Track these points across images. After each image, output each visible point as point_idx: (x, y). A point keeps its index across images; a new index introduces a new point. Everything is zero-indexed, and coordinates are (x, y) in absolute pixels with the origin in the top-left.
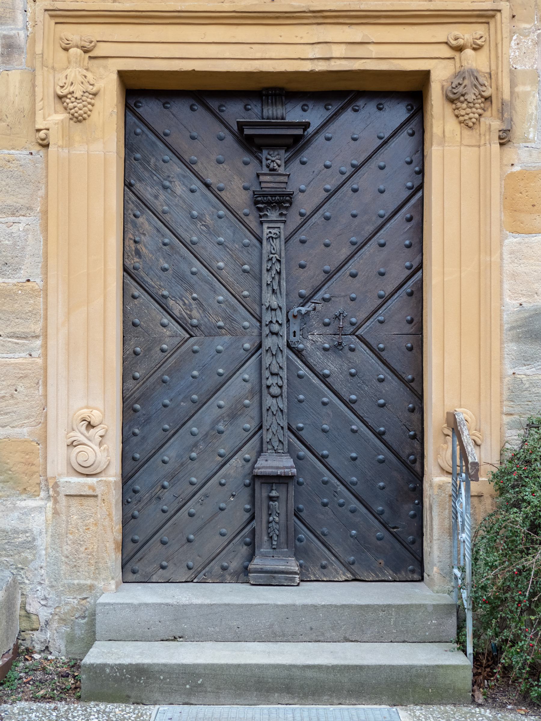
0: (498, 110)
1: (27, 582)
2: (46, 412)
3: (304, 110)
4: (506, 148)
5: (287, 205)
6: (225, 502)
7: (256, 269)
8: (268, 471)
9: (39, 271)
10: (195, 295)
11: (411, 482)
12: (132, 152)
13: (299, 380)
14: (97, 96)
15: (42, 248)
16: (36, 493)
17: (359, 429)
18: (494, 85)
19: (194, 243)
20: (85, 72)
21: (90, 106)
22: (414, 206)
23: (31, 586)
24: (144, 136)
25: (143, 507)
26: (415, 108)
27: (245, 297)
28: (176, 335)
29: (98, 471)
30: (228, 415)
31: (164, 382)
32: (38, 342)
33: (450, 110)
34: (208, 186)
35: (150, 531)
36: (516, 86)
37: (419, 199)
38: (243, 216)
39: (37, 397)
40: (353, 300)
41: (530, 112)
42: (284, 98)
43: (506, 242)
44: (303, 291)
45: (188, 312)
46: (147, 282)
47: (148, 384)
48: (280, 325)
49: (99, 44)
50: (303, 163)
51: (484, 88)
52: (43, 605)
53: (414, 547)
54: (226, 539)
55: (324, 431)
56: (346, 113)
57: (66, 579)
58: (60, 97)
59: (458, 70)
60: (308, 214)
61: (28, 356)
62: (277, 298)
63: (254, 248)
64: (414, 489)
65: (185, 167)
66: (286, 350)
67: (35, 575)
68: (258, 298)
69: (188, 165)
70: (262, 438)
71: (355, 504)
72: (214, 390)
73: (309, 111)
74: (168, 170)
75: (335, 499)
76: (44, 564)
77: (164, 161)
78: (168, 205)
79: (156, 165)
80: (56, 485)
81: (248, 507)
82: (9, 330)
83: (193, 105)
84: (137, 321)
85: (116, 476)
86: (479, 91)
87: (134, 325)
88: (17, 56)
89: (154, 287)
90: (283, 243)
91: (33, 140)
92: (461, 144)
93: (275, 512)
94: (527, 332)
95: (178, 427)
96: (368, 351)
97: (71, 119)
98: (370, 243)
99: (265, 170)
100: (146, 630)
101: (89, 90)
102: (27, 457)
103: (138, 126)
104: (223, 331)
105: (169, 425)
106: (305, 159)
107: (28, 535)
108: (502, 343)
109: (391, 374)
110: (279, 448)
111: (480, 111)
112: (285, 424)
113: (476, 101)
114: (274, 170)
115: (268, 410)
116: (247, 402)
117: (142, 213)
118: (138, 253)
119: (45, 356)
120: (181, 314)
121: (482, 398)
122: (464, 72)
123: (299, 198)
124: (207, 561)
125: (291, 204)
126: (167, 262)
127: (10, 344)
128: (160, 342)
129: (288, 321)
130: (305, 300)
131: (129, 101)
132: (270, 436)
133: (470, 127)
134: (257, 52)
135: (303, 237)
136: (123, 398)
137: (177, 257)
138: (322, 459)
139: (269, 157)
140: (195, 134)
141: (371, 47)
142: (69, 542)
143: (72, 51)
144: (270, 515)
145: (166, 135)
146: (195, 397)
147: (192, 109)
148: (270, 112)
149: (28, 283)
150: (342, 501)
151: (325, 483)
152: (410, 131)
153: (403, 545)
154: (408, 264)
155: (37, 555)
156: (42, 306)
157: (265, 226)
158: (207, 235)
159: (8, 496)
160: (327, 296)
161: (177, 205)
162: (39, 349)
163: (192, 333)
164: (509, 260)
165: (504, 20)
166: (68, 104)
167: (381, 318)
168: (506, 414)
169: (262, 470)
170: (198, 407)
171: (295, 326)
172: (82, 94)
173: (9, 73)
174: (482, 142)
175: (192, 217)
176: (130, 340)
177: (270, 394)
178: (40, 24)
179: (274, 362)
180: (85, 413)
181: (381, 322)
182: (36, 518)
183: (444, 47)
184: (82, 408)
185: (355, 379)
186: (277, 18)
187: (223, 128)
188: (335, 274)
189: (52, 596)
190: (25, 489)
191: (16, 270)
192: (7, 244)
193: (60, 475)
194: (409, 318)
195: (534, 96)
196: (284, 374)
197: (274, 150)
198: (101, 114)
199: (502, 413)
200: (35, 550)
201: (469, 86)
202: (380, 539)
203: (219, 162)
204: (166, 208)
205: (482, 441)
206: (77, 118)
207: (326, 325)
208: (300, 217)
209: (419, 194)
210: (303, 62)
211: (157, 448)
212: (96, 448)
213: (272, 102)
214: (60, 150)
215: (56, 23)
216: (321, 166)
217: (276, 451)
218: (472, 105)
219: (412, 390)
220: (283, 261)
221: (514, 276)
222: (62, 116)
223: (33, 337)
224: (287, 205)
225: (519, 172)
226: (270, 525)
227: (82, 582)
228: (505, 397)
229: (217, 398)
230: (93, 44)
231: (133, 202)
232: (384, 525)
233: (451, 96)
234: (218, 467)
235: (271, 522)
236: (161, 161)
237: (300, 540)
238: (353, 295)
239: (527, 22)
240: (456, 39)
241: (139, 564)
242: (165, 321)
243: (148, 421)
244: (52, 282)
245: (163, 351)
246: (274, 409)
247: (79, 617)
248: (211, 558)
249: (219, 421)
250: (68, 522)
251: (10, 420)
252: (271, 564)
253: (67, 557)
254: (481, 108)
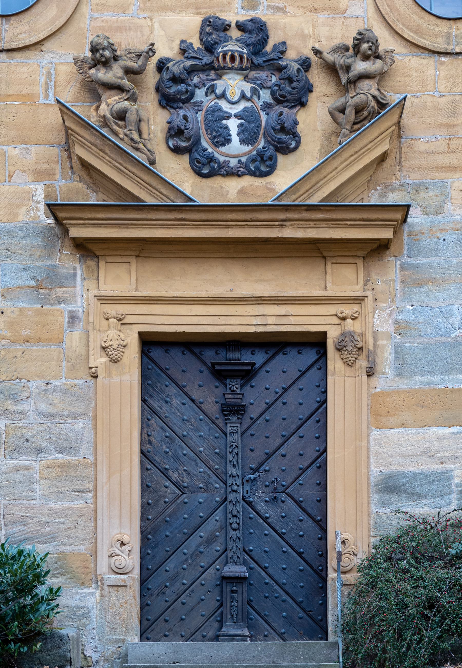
0: (366, 356)
1: (85, 637)
2: (96, 537)
3: (253, 354)
4: (372, 379)
5: (242, 412)
6: (204, 595)
7: (223, 453)
8: (231, 574)
9: (91, 452)
10: (185, 468)
11: (320, 583)
12: (146, 380)
13: (250, 520)
14: (126, 348)
15: (93, 438)
16: (89, 585)
17: (287, 550)
18: (364, 341)
19: (184, 436)
20: (119, 333)
21: (122, 353)
22: (321, 413)
23: (87, 640)
24: (153, 370)
25: (153, 599)
26: (322, 352)
27: (216, 469)
28: (173, 493)
29: (128, 571)
30: (206, 542)
31: (166, 521)
32: (91, 495)
33: (339, 355)
34: (193, 401)
35: (158, 614)
36: (378, 341)
37: (324, 409)
38: (215, 419)
39: (90, 527)
40: (283, 471)
41: (386, 356)
42: (239, 347)
43: (372, 434)
44: (252, 466)
45: (181, 479)
46: (156, 460)
47: (156, 523)
48: (238, 486)
49: (127, 316)
50: (252, 387)
51: (357, 343)
52: (94, 651)
53: (322, 623)
54: (205, 619)
55: (266, 551)
56: (279, 356)
57: (108, 636)
58: (104, 348)
59: (343, 331)
60: (255, 418)
61: (85, 503)
62: (236, 469)
63: (222, 439)
64: (322, 588)
65: (179, 389)
66: (241, 502)
67: (89, 633)
68: (224, 470)
69: (181, 388)
70: (227, 556)
71: (285, 597)
72: (198, 527)
73: (256, 354)
74: (169, 391)
75: (273, 594)
76: (95, 627)
77: (166, 386)
78: (168, 413)
79: (161, 388)
80: (102, 579)
81: (218, 598)
82: (73, 487)
83: (184, 351)
84: (149, 484)
85: (138, 575)
86: (355, 344)
87: (148, 486)
88: (77, 323)
89: (160, 463)
90: (239, 436)
91: (88, 373)
92: (345, 376)
93: (235, 600)
94: (385, 487)
95: (175, 549)
96: (293, 502)
97: (110, 361)
98: (294, 436)
99: (229, 391)
100: (158, 658)
101: (121, 344)
102: (84, 563)
103: (150, 364)
104: (203, 490)
105: (170, 548)
106: (253, 384)
107: (85, 609)
108: (369, 494)
109: (307, 516)
110: (238, 561)
111: (355, 356)
112: (241, 546)
113: (353, 350)
114: (233, 391)
115: (230, 538)
116: (218, 533)
117: (152, 418)
118: (150, 442)
119: (95, 503)
120: (177, 480)
121: (357, 527)
122: (346, 333)
123: (250, 408)
124: (193, 632)
125: (245, 412)
126: (168, 448)
127: (74, 496)
128: (164, 497)
129: (243, 484)
130: (254, 471)
131: (144, 349)
132: (232, 554)
133: (350, 366)
134: (222, 320)
135: (252, 432)
136: (141, 532)
137: (174, 445)
138: (265, 569)
139: (231, 383)
140: (185, 369)
141: (291, 318)
142: (110, 614)
143: (111, 320)
144: (232, 602)
145: (167, 369)
146: (185, 531)
147: (183, 354)
148: (231, 356)
149: (85, 459)
150: (277, 595)
151: (266, 584)
152: (319, 367)
153: (315, 622)
154: (317, 448)
155: (91, 621)
156: (93, 473)
157: (229, 425)
158: (193, 431)
159: (73, 587)
160: (267, 468)
161: (174, 413)
162: (91, 499)
163: (184, 491)
164: (374, 444)
165: (369, 302)
166: (108, 352)
167: (301, 482)
168: (373, 537)
169: (227, 574)
170: (187, 537)
171: (248, 487)
172: (117, 346)
173: (73, 333)
174: (357, 374)
175: (184, 420)
176: (145, 496)
177: (232, 528)
178: (92, 305)
179: (234, 509)
180: (119, 536)
181: (301, 484)
182: (90, 599)
183: (335, 318)
184: (118, 534)
185: (285, 519)
186: (234, 301)
187: (203, 365)
188: (272, 455)
189: (100, 645)
190: (83, 583)
191: (78, 451)
192: (72, 436)
193: (104, 573)
194: (318, 482)
195: (388, 347)
196: (240, 516)
197: (234, 379)
198: (129, 358)
199: (369, 536)
200: (90, 618)
201: (349, 342)
202: (301, 618)
203: (200, 386)
204: (167, 414)
205: (358, 552)
206: (114, 360)
207: (267, 486)
208: (250, 420)
209: (325, 405)
210: (250, 326)
211: (162, 562)
212: (126, 557)
213: (232, 350)
214: (104, 379)
215: (101, 303)
216: (263, 388)
217: (236, 563)
218: (350, 352)
219: (321, 527)
220: (240, 447)
221: (377, 454)
222: (104, 359)
223: (87, 491)
224: (242, 412)
225: (380, 392)
226: (232, 608)
227: (118, 637)
228: (371, 526)
229: (199, 532)
230: (123, 316)
231: (147, 411)
232: (303, 610)
233: (338, 347)
234: (200, 574)
235: (233, 606)
236: (164, 386)
237: (251, 619)
238: (284, 468)
239: (385, 303)
240: (342, 313)
241: (151, 634)
242: (167, 484)
243: (156, 546)
244: (99, 458)
245: (165, 502)
246: (234, 537)
247: (116, 658)
248: (196, 630)
249: (200, 546)
250: (109, 601)
251: (74, 541)
252: (232, 631)
253: (109, 623)
254: (356, 354)
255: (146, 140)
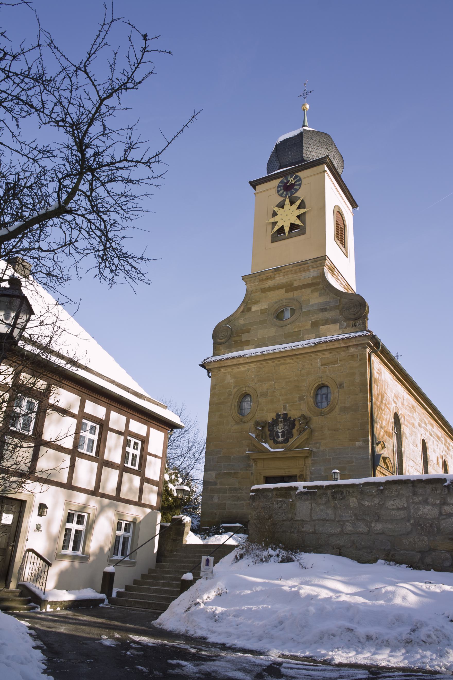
255: (108, 182)
